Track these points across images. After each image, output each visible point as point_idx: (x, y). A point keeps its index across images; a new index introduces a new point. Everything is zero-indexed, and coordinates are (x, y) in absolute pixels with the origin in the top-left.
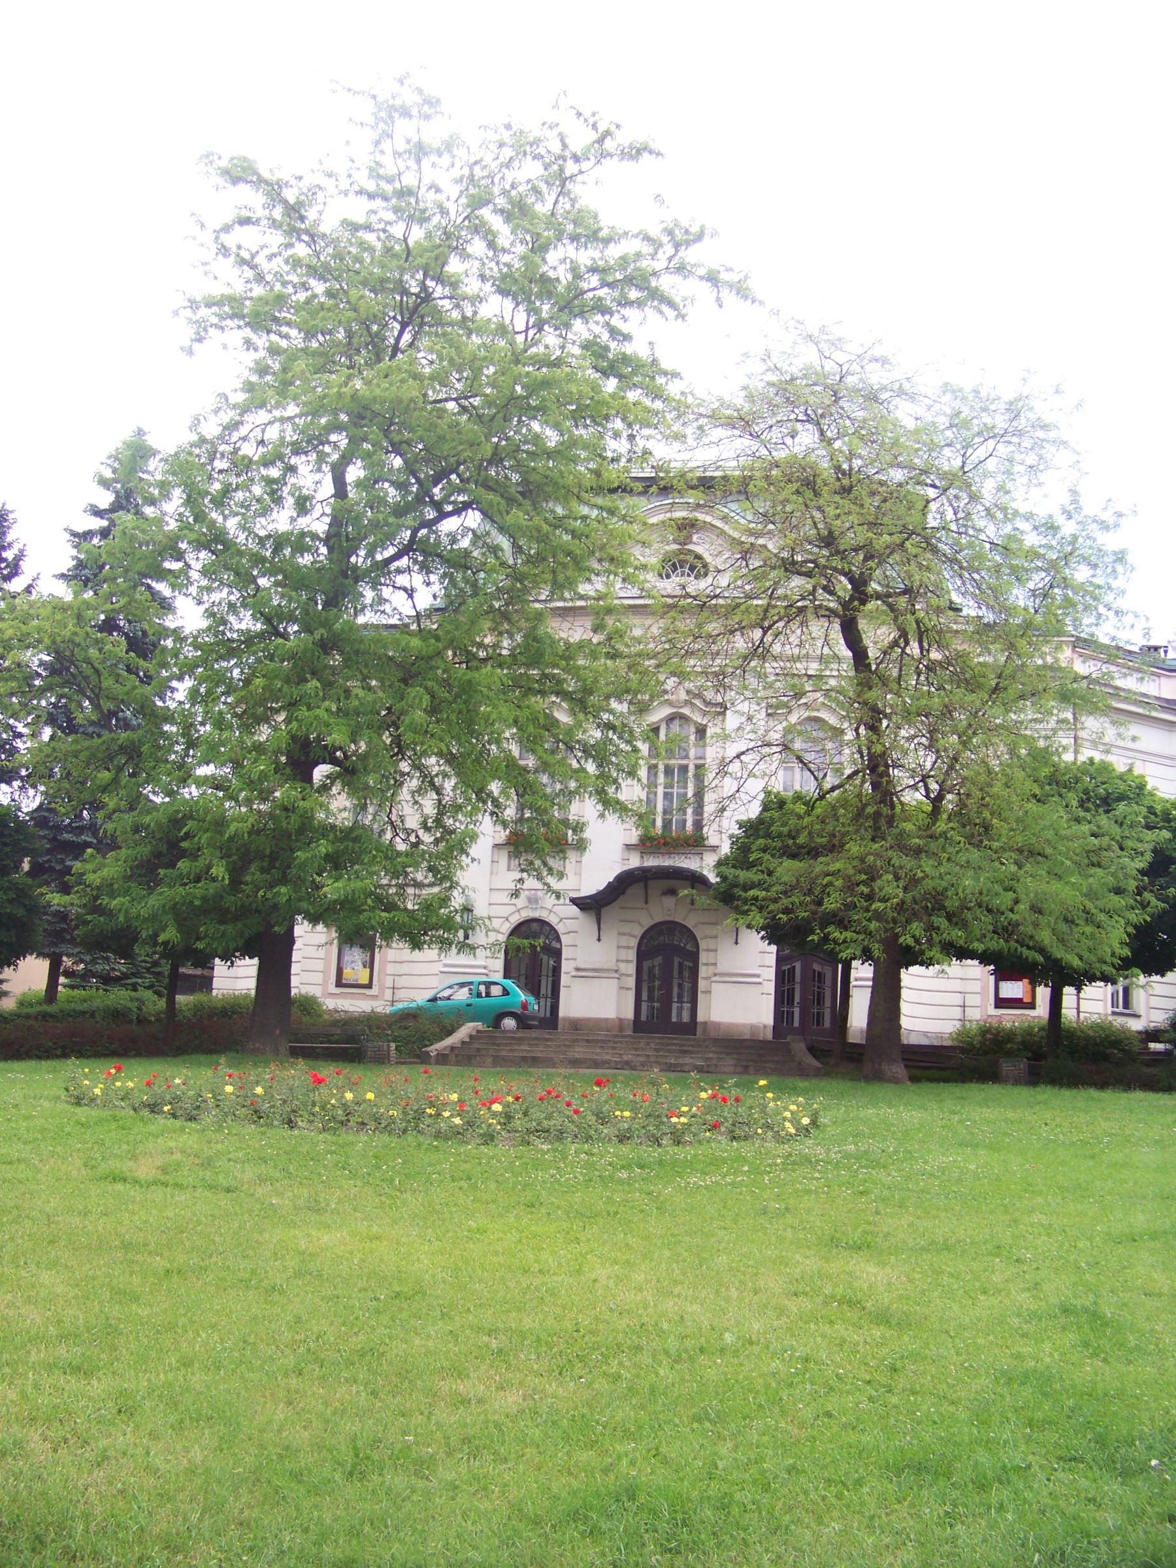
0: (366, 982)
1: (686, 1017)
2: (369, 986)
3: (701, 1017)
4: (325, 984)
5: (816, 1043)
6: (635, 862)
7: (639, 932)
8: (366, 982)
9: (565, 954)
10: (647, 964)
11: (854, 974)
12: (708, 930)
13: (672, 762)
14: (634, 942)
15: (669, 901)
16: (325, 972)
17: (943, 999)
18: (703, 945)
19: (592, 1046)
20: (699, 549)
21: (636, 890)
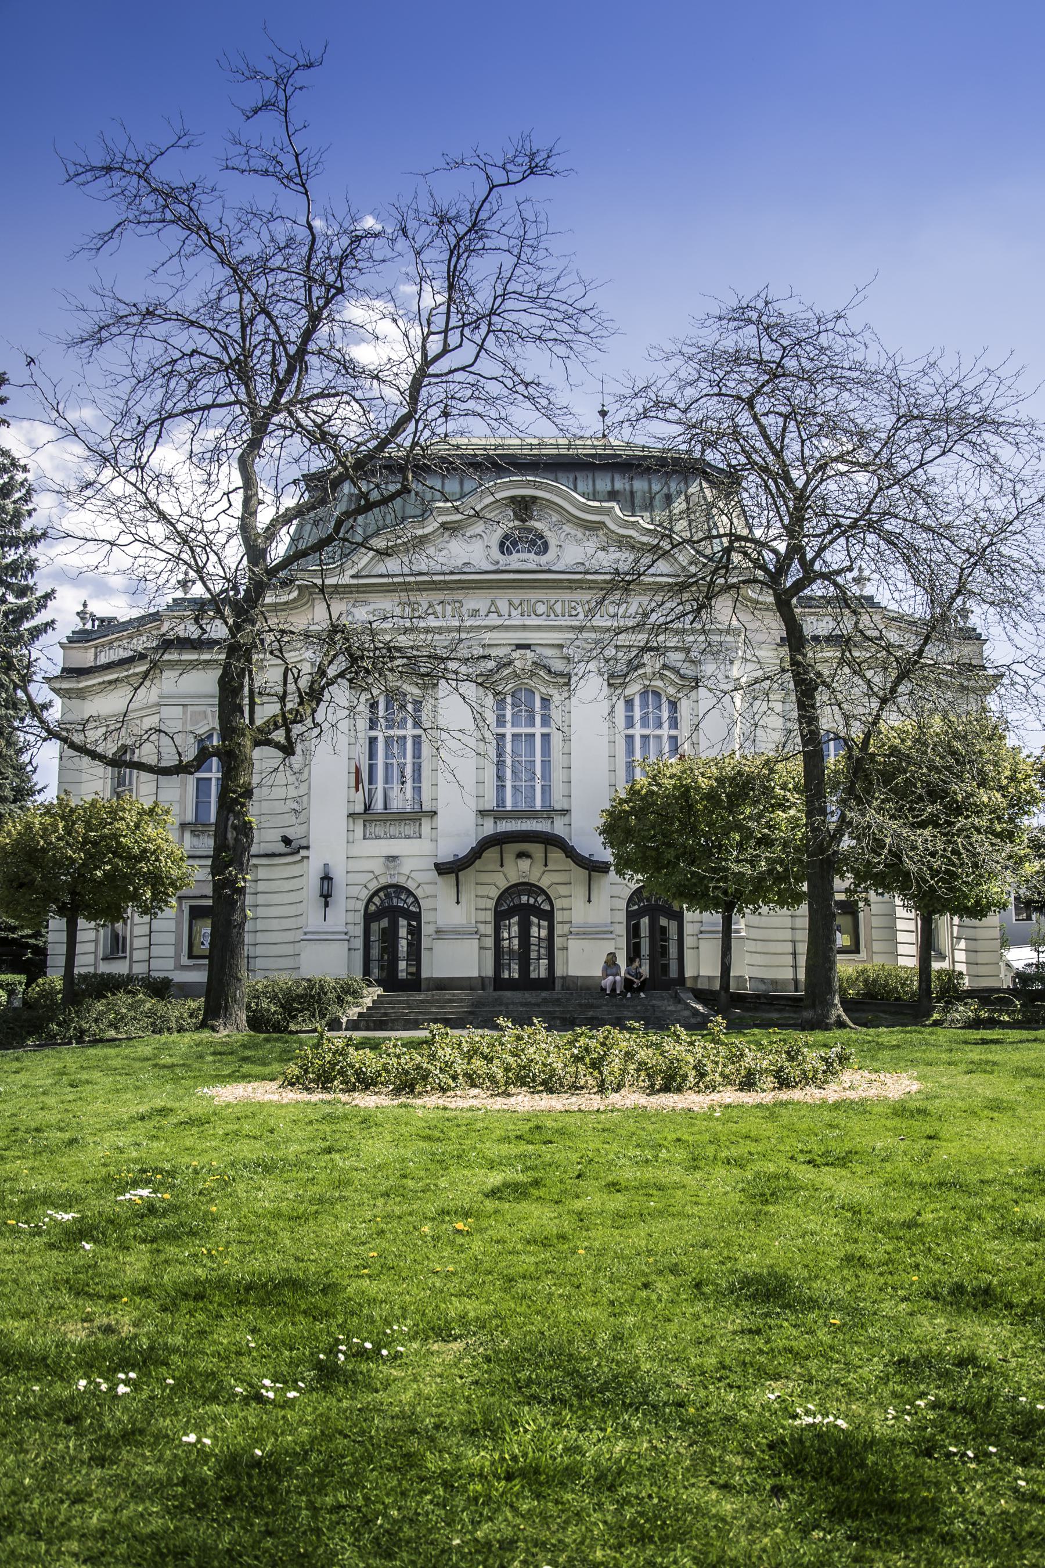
0: (195, 953)
1: (543, 974)
2: (857, 951)
3: (559, 972)
4: (177, 956)
5: (651, 991)
6: (489, 828)
7: (495, 893)
8: (195, 953)
9: (424, 918)
10: (374, 926)
11: (81, 936)
12: (563, 890)
13: (391, 732)
14: (491, 904)
15: (524, 864)
16: (177, 945)
17: (769, 944)
18: (558, 904)
19: (574, 1007)
20: (538, 525)
21: (491, 855)
